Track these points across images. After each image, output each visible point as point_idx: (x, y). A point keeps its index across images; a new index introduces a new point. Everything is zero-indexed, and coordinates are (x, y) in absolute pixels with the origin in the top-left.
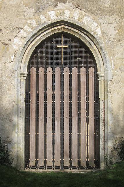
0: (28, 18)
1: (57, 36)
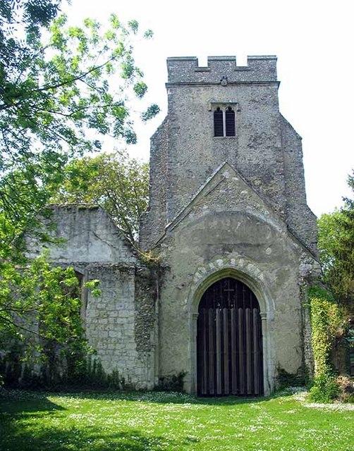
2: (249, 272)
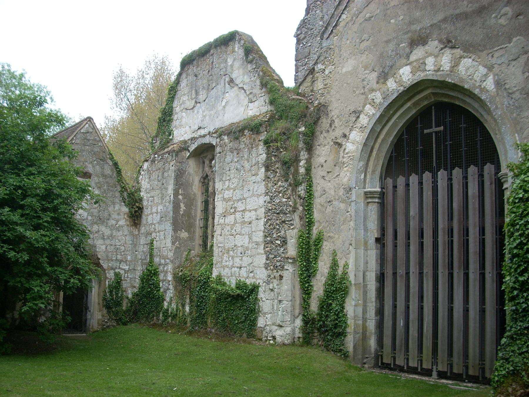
0: (370, 91)
2: (462, 80)
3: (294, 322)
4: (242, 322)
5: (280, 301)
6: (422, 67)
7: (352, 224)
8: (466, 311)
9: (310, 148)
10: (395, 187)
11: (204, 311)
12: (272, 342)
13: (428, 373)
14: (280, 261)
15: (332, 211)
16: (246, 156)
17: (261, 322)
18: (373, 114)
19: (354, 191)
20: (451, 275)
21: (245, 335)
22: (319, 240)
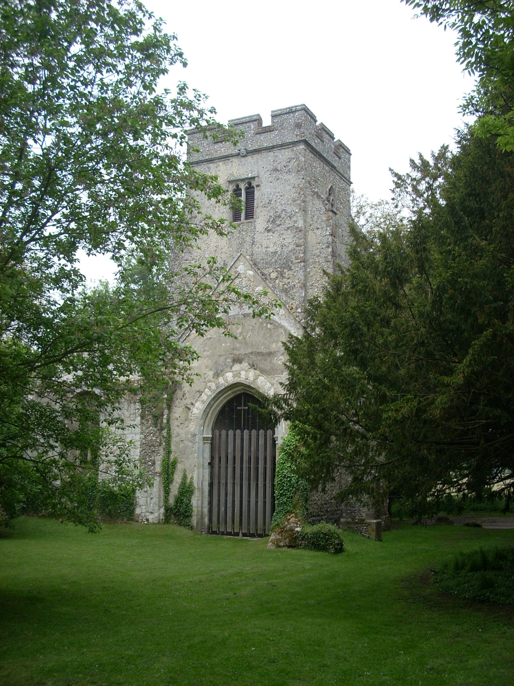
1: (230, 403)
3: (159, 510)
4: (124, 511)
5: (152, 498)
6: (239, 375)
7: (196, 455)
8: (257, 502)
9: (169, 407)
10: (220, 435)
11: (92, 505)
12: (146, 522)
13: (237, 534)
14: (151, 474)
15: (184, 447)
16: (126, 407)
17: (138, 511)
18: (210, 395)
19: (197, 436)
20: (249, 484)
21: (125, 519)
22: (174, 464)
